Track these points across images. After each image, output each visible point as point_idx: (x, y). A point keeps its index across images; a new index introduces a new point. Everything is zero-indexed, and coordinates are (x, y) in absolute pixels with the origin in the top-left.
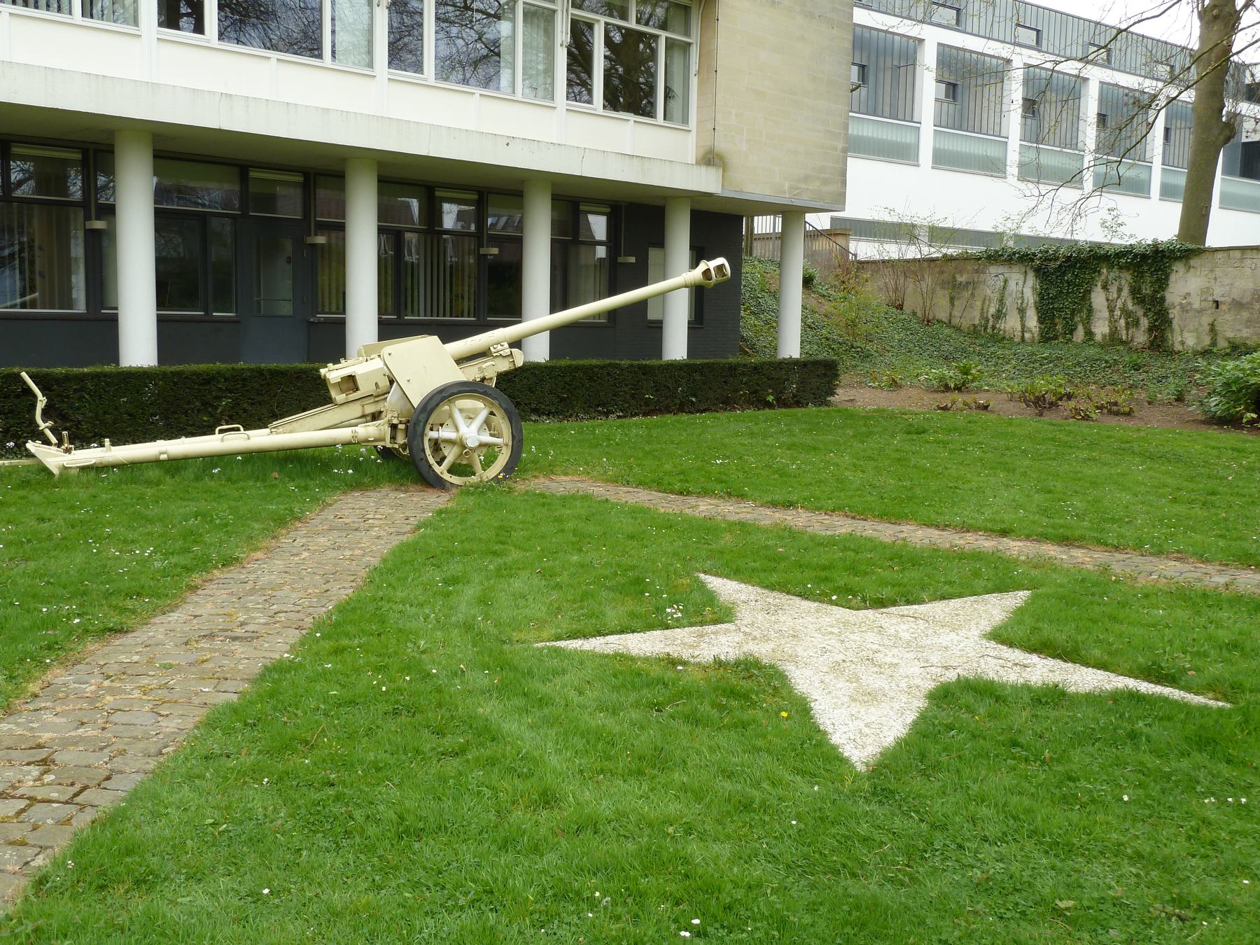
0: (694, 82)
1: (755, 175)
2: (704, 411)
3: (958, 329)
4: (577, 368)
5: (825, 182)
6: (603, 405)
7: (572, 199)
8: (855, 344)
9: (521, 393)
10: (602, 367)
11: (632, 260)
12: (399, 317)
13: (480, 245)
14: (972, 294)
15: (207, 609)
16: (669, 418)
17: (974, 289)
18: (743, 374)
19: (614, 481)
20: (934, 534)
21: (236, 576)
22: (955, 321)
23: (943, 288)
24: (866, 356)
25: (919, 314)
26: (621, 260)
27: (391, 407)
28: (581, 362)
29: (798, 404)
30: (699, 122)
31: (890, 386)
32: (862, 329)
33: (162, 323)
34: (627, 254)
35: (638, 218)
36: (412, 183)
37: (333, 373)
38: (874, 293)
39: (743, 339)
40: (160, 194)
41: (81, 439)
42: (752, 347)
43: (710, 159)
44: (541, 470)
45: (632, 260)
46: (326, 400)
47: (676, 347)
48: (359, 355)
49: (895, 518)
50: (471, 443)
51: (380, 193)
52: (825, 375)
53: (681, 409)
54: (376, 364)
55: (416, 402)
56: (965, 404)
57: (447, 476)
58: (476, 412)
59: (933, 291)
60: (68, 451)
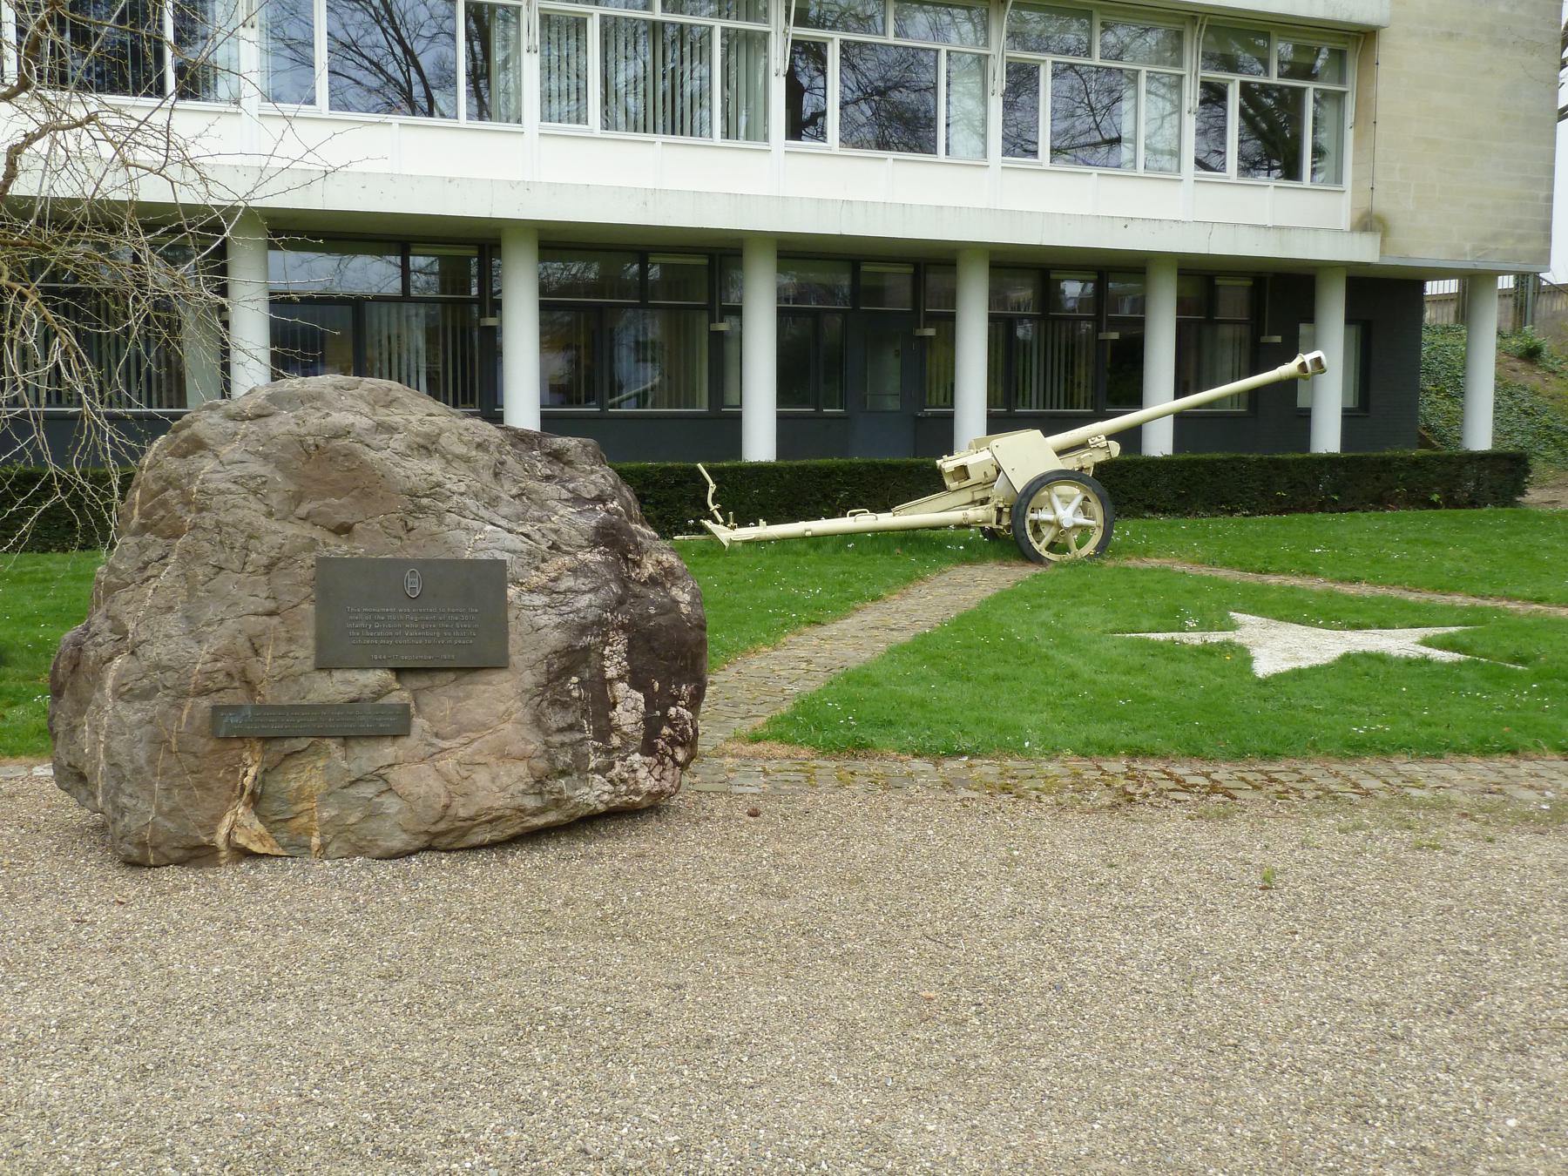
0: (1349, 135)
1: (1430, 236)
4: (1197, 463)
5: (1522, 239)
6: (1227, 502)
7: (1203, 280)
9: (1125, 486)
11: (1278, 339)
12: (1009, 409)
13: (1099, 329)
15: (869, 618)
16: (1297, 518)
18: (1401, 469)
19: (1202, 562)
20: (1473, 600)
26: (1264, 339)
27: (998, 493)
28: (1202, 456)
29: (1473, 504)
30: (1355, 181)
33: (781, 419)
34: (1271, 334)
35: (1252, 304)
36: (1026, 272)
37: (947, 464)
40: (781, 297)
41: (743, 523)
43: (1368, 223)
44: (1134, 553)
45: (1278, 339)
46: (944, 488)
47: (1327, 438)
48: (970, 447)
50: (1067, 524)
51: (991, 275)
52: (1512, 471)
53: (1321, 508)
54: (985, 455)
55: (1019, 487)
57: (1045, 554)
58: (1073, 497)
60: (733, 528)
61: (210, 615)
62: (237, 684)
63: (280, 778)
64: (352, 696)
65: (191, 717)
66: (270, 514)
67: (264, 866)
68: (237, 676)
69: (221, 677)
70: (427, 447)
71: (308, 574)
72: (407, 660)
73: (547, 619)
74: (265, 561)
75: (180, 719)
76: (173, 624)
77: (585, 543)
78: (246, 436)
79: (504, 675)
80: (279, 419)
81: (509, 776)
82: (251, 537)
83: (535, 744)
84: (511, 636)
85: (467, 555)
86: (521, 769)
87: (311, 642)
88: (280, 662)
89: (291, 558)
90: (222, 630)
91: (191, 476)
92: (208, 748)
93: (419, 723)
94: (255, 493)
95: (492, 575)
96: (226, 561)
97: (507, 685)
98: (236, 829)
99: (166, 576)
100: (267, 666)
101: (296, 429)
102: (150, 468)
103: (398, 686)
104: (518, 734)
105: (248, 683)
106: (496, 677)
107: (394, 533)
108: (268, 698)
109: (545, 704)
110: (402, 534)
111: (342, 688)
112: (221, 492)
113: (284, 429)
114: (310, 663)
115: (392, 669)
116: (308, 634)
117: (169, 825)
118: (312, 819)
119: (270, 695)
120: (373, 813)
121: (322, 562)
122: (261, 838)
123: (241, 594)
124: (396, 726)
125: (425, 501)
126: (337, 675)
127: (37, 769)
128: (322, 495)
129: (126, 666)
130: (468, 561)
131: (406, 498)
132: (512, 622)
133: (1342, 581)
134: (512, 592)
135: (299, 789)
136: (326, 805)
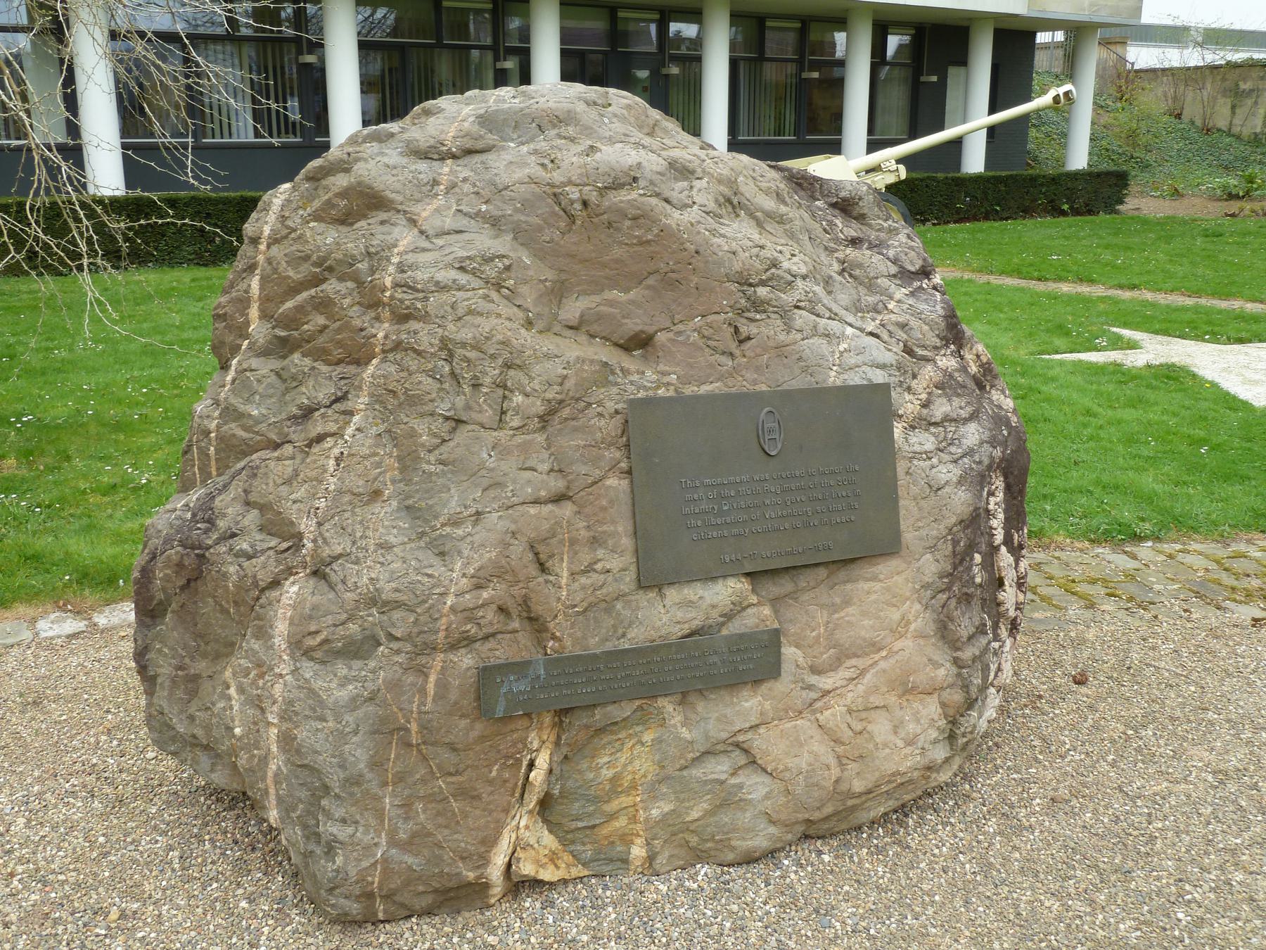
2: (1007, 219)
3: (1238, 137)
6: (921, 214)
8: (1135, 155)
10: (921, 180)
11: (934, 79)
13: (802, 70)
14: (1256, 103)
17: (1258, 97)
18: (1042, 185)
21: (241, 433)
22: (1236, 130)
23: (1224, 96)
24: (1145, 167)
25: (1199, 123)
26: (923, 79)
31: (1172, 195)
32: (1143, 140)
38: (1153, 101)
39: (1029, 153)
42: (1035, 159)
45: (934, 79)
49: (1227, 296)
56: (1253, 211)
59: (1215, 99)
61: (453, 506)
62: (516, 624)
63: (584, 765)
64: (696, 624)
65: (442, 685)
66: (529, 324)
67: (562, 901)
68: (515, 612)
69: (490, 614)
71: (611, 427)
73: (946, 472)
74: (539, 407)
75: (423, 691)
76: (384, 520)
77: (938, 342)
78: (454, 186)
79: (893, 563)
80: (506, 157)
81: (918, 721)
82: (508, 366)
83: (945, 672)
84: (902, 503)
85: (833, 378)
86: (931, 708)
87: (627, 542)
88: (583, 580)
90: (480, 535)
91: (376, 257)
92: (474, 734)
94: (498, 286)
95: (871, 405)
96: (468, 407)
97: (899, 579)
98: (520, 854)
99: (359, 429)
100: (563, 589)
101: (540, 172)
102: (274, 241)
103: (754, 599)
106: (884, 568)
107: (721, 346)
109: (953, 602)
110: (733, 346)
111: (680, 615)
112: (442, 288)
113: (520, 174)
114: (630, 576)
115: (748, 575)
116: (621, 531)
117: (410, 860)
118: (633, 819)
119: (569, 637)
120: (727, 799)
122: (553, 858)
123: (504, 466)
124: (756, 661)
125: (762, 292)
126: (672, 594)
127: (41, 625)
128: (596, 287)
129: (312, 600)
131: (734, 287)
132: (902, 479)
133: (1121, 287)
134: (898, 430)
135: (615, 779)
136: (655, 798)
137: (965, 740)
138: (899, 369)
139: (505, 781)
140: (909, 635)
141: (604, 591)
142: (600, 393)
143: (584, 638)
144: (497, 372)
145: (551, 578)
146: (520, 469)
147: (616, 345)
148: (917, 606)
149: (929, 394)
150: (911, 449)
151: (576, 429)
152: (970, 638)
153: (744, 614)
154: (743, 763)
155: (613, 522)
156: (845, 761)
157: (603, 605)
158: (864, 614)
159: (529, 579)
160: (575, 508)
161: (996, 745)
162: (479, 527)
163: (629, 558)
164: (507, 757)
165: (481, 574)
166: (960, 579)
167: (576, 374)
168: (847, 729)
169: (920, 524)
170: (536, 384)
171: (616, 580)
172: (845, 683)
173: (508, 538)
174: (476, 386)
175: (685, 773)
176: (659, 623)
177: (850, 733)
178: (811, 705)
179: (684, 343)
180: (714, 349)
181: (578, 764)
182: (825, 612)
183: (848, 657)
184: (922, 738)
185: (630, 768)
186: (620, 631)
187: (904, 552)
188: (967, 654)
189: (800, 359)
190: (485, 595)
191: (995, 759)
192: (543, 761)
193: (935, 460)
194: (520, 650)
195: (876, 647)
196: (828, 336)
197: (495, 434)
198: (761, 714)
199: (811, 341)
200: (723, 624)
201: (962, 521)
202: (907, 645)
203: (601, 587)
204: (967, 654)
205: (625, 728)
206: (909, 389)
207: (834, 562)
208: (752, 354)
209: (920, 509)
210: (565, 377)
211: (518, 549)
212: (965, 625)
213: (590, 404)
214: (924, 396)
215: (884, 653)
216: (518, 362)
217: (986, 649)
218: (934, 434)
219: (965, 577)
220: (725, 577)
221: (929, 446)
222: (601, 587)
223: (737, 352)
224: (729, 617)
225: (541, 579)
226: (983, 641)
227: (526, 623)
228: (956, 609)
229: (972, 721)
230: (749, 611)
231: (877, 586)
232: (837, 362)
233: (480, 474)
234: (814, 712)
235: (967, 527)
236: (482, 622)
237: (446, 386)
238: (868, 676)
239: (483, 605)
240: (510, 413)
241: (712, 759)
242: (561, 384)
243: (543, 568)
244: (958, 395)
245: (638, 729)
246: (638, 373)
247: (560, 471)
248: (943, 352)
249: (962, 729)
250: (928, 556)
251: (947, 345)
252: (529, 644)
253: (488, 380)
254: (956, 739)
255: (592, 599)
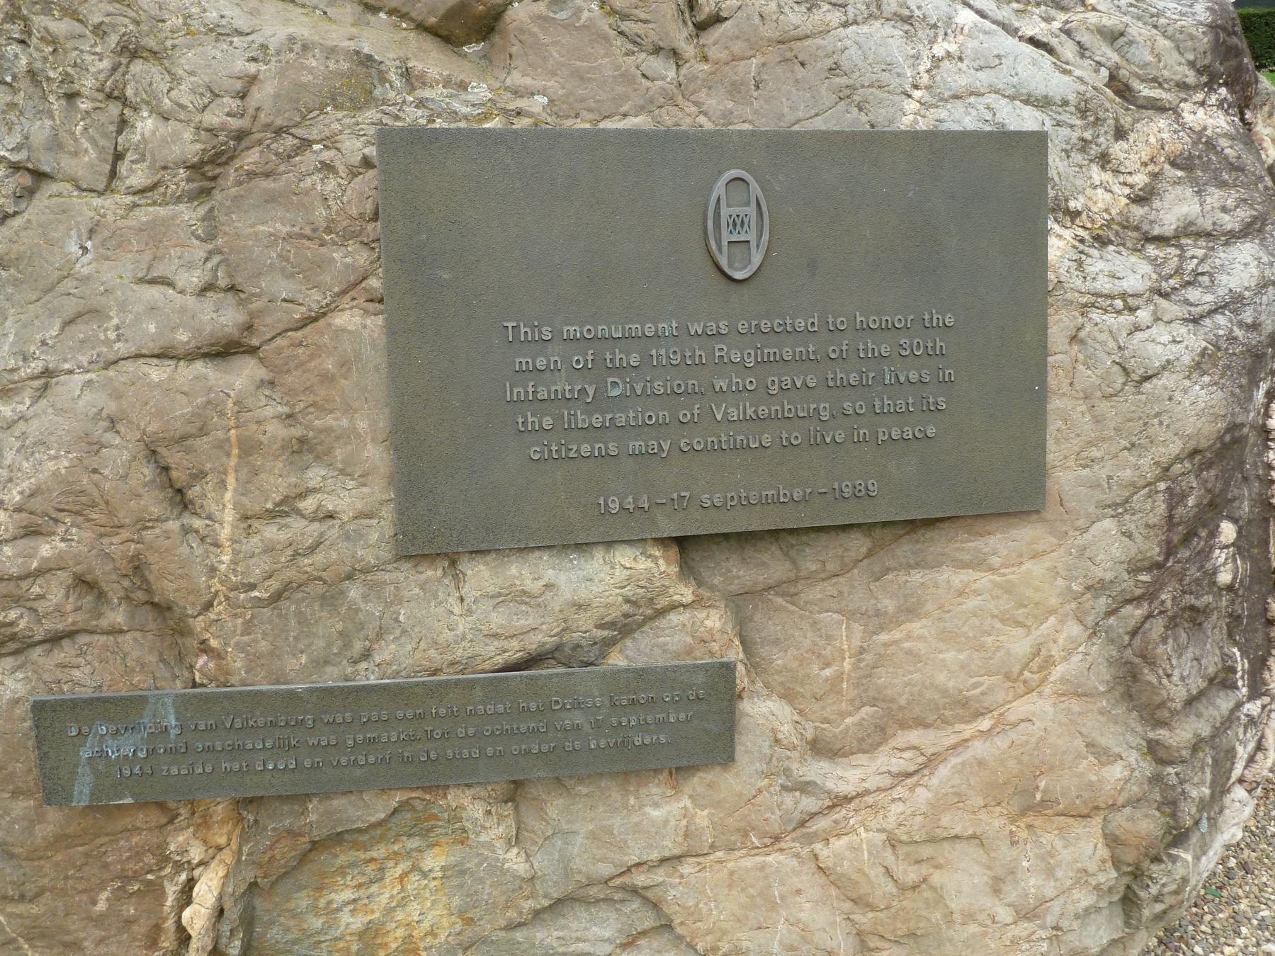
10: (1260, 17)
62: (118, 617)
63: (302, 901)
64: (534, 642)
68: (115, 592)
69: (55, 592)
70: (81, 793)
71: (356, 195)
72: (714, 503)
73: (1167, 341)
74: (188, 146)
77: (1191, 78)
79: (1026, 534)
81: (1050, 872)
82: (130, 51)
83: (1123, 771)
85: (910, 115)
86: (1085, 847)
87: (375, 455)
88: (270, 532)
89: (287, 134)
90: (44, 419)
92: (44, 831)
93: (763, 712)
95: (996, 184)
96: (55, 144)
97: (1035, 569)
100: (224, 544)
103: (685, 593)
104: (1059, 718)
105: (161, 608)
106: (1000, 543)
107: (651, 34)
108: (237, 663)
109: (1157, 627)
110: (680, 36)
111: (497, 620)
114: (380, 531)
115: (663, 542)
116: (364, 427)
119: (238, 652)
121: (403, 149)
124: (687, 725)
126: (481, 576)
130: (915, 137)
132: (1060, 353)
134: (1060, 244)
137: (1159, 907)
138: (1083, 113)
139: (129, 922)
140: (1047, 690)
141: (319, 558)
142: (334, 120)
143: (274, 654)
144: (106, 64)
145: (197, 523)
146: (141, 281)
147: (421, 27)
148: (1074, 629)
149: (1155, 176)
150: (1089, 285)
151: (271, 198)
152: (1190, 702)
153: (663, 622)
154: (648, 924)
155: (348, 409)
156: (873, 942)
157: (319, 588)
158: (948, 637)
159: (143, 524)
160: (262, 373)
161: (1244, 866)
162: (43, 403)
163: (377, 492)
164: (126, 879)
165: (36, 504)
166: (1180, 577)
167: (281, 73)
168: (883, 880)
169: (1096, 453)
170: (183, 94)
171: (348, 538)
172: (887, 781)
173: (99, 430)
174: (71, 97)
175: (519, 935)
176: (448, 635)
177: (891, 888)
178: (802, 824)
179: (568, 26)
180: (636, 41)
181: (288, 900)
182: (858, 628)
183: (904, 725)
184: (1056, 907)
185: (400, 915)
186: (358, 646)
187: (1052, 511)
188: (1180, 735)
189: (835, 69)
190: (46, 550)
191: (1237, 899)
192: (208, 889)
193: (1144, 315)
194: (129, 671)
195: (968, 708)
196: (908, 20)
197: (97, 201)
198: (686, 836)
199: (864, 29)
200: (609, 643)
201: (1196, 452)
202: (1039, 709)
203: (312, 549)
204: (1180, 735)
205: (382, 838)
206: (1104, 160)
207: (885, 524)
208: (724, 56)
209: (1097, 420)
210: (253, 79)
211: (119, 453)
212: (1181, 671)
213: (306, 143)
214: (1140, 179)
215: (985, 724)
216: (150, 42)
217: (1230, 720)
218: (1152, 261)
219: (1194, 572)
220: (609, 544)
221: (1133, 283)
222: (312, 549)
223: (689, 50)
224: (623, 628)
225: (173, 525)
226: (1224, 703)
227: (147, 615)
228: (1164, 640)
229: (1180, 871)
230: (675, 618)
231: (984, 580)
232: (925, 79)
233: (62, 288)
234: (810, 839)
235: (1209, 465)
236: (41, 606)
237: (20, 98)
238: (943, 771)
239: (39, 573)
240: (130, 156)
241: (583, 913)
242: (243, 96)
243: (181, 499)
244: (1223, 185)
245: (414, 843)
246: (447, 83)
247: (232, 288)
248: (1199, 96)
249: (1154, 890)
250: (1108, 523)
251: (1210, 86)
252: (152, 658)
253: (87, 84)
254: (1139, 907)
255: (289, 574)
